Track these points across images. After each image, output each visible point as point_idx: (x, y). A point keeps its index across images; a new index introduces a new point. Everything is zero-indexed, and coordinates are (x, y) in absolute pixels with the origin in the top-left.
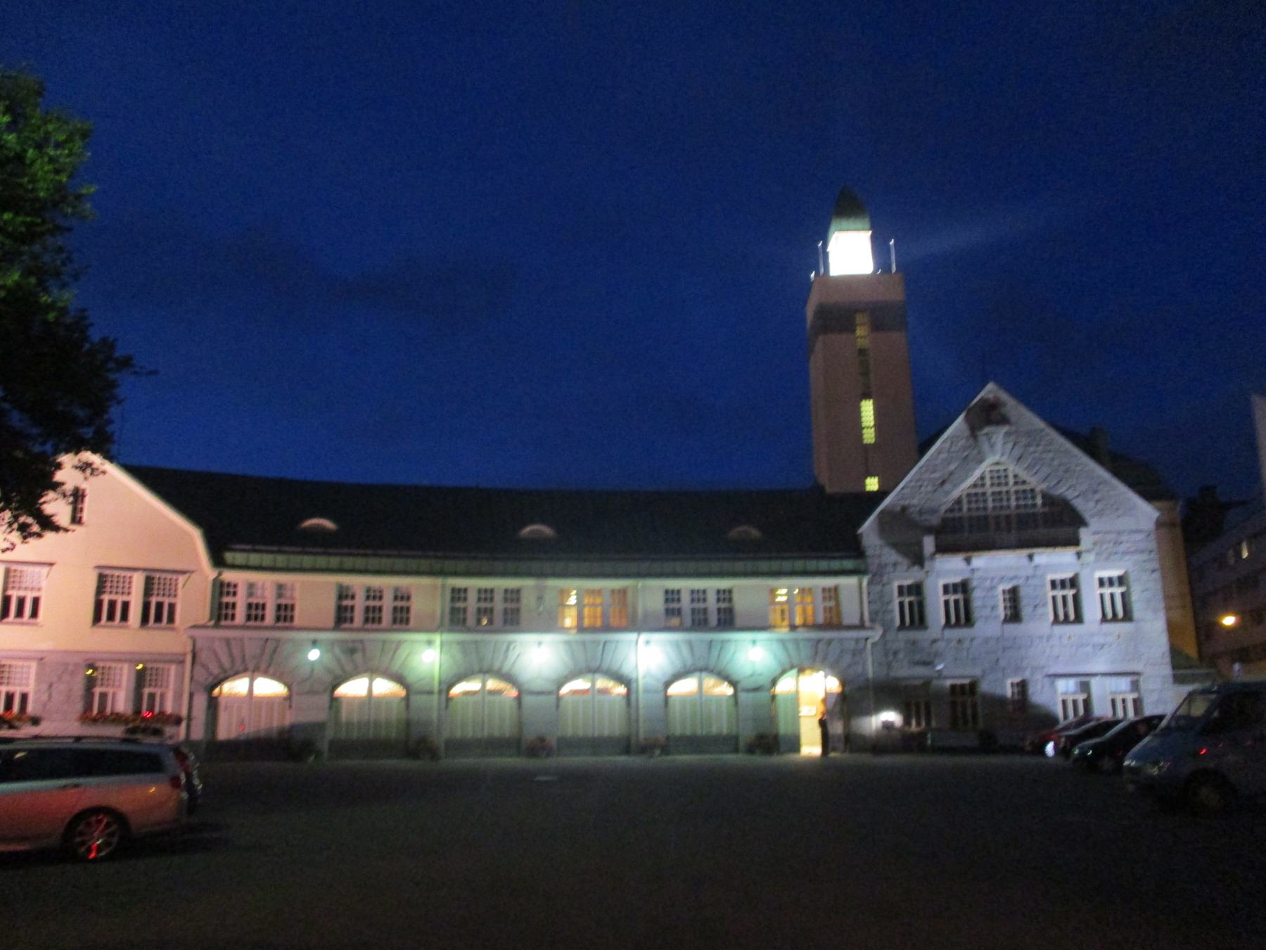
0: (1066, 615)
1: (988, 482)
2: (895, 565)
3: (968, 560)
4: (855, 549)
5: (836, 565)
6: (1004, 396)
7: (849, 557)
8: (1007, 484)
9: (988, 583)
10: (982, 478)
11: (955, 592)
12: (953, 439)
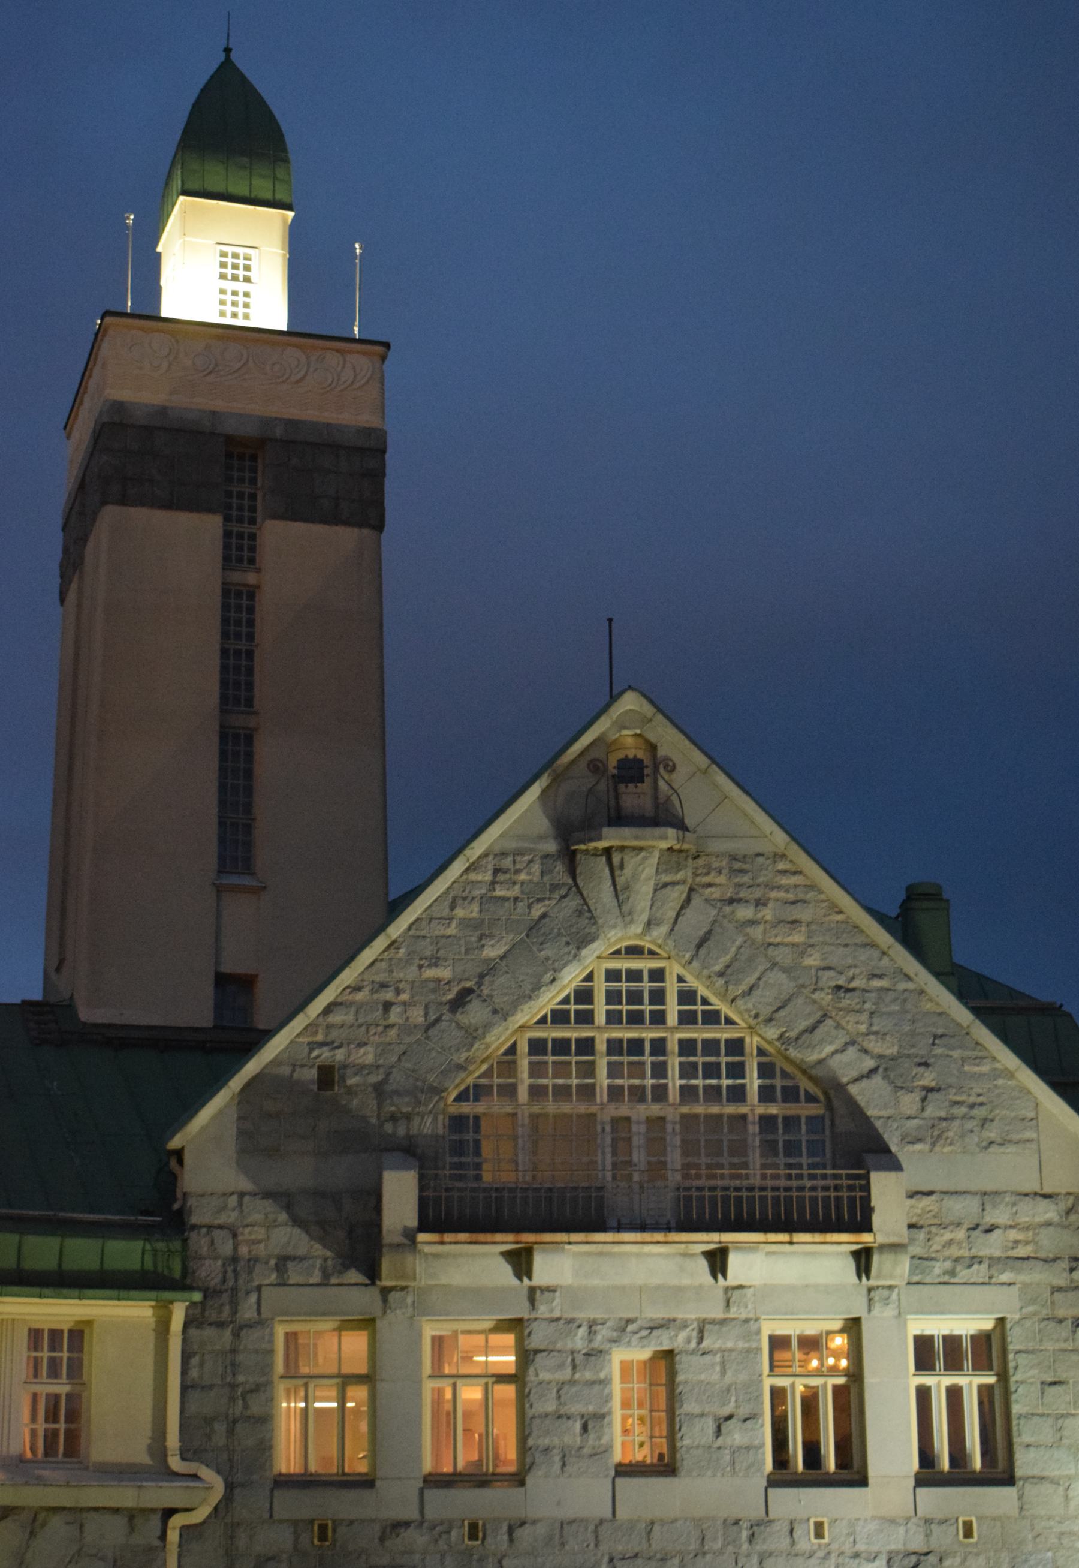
0: (958, 1455)
1: (600, 1008)
2: (283, 1262)
3: (521, 1262)
4: (161, 1208)
5: (82, 1253)
6: (671, 742)
7: (129, 1230)
8: (659, 1018)
9: (579, 1340)
10: (584, 995)
11: (953, 1364)
12: (500, 865)
